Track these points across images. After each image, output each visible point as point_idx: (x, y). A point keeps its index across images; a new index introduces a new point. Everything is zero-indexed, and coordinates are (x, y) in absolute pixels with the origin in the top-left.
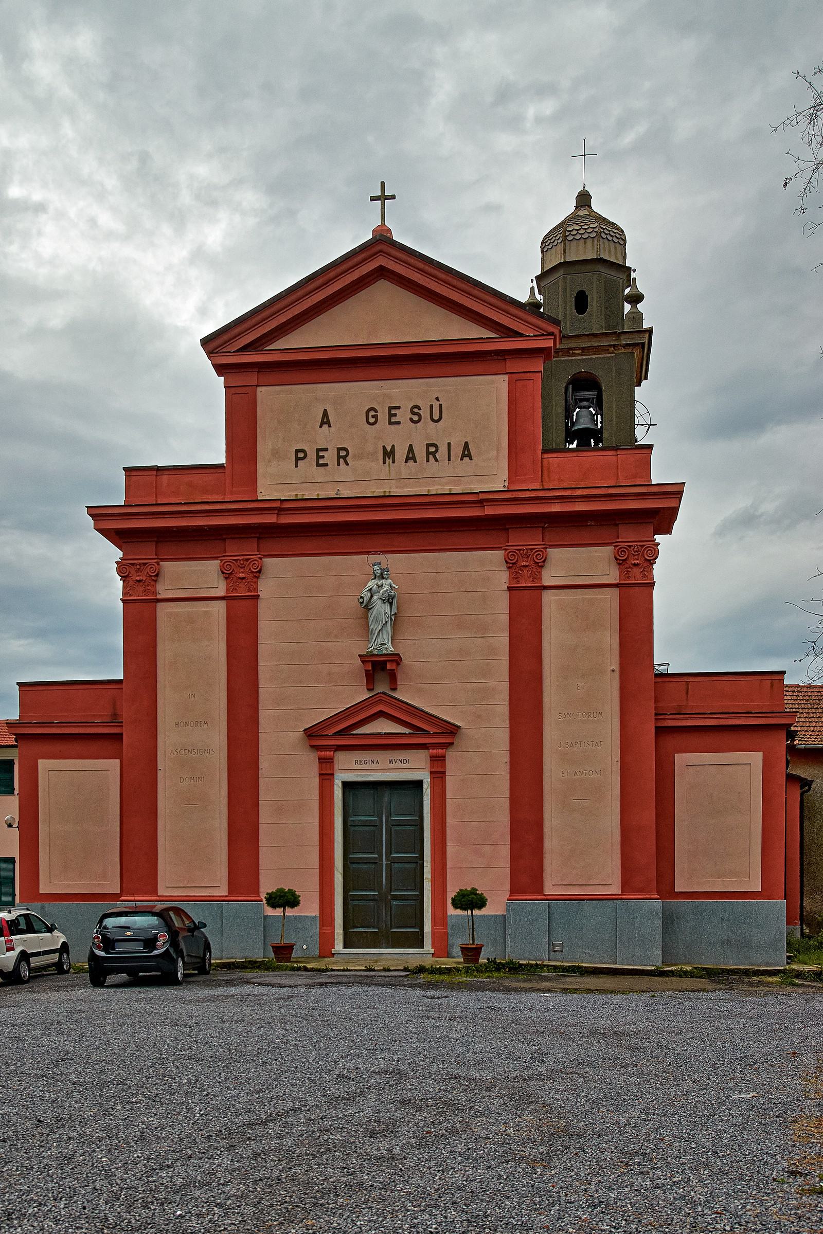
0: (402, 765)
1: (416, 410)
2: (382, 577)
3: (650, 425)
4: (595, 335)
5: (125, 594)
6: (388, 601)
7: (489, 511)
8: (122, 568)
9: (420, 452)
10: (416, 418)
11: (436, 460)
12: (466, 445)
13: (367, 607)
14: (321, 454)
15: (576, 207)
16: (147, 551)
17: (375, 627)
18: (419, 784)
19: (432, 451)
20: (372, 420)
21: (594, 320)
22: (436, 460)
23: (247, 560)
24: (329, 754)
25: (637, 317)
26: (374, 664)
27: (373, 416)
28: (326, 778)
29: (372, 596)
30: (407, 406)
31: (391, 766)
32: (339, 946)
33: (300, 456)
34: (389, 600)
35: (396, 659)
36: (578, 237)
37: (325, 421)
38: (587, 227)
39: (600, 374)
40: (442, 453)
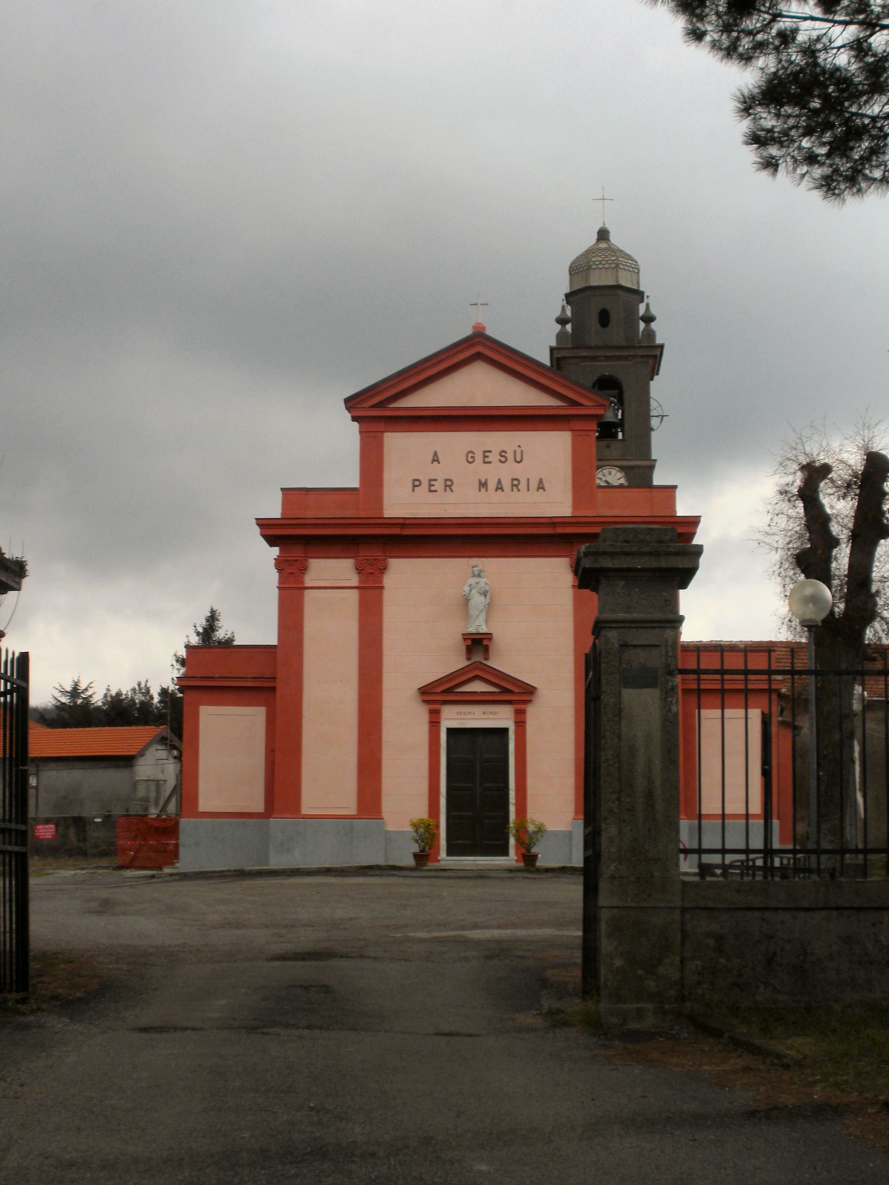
0: (492, 716)
1: (503, 454)
2: (479, 576)
3: (663, 416)
4: (618, 348)
5: (280, 582)
6: (484, 594)
7: (560, 530)
8: (280, 564)
9: (507, 484)
10: (503, 459)
11: (519, 491)
12: (541, 481)
13: (467, 600)
14: (432, 483)
15: (598, 240)
16: (297, 552)
17: (473, 612)
18: (505, 731)
19: (515, 484)
20: (471, 460)
21: (615, 334)
22: (519, 491)
23: (376, 559)
24: (436, 707)
25: (650, 335)
26: (473, 640)
27: (472, 457)
28: (434, 724)
29: (471, 590)
30: (496, 451)
31: (484, 716)
32: (443, 854)
33: (416, 484)
34: (485, 594)
35: (489, 636)
36: (600, 266)
37: (436, 459)
38: (608, 259)
39: (621, 376)
40: (523, 486)
